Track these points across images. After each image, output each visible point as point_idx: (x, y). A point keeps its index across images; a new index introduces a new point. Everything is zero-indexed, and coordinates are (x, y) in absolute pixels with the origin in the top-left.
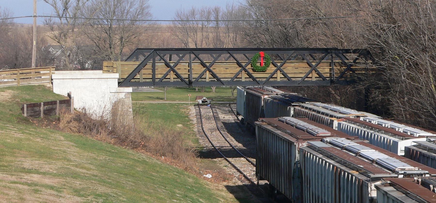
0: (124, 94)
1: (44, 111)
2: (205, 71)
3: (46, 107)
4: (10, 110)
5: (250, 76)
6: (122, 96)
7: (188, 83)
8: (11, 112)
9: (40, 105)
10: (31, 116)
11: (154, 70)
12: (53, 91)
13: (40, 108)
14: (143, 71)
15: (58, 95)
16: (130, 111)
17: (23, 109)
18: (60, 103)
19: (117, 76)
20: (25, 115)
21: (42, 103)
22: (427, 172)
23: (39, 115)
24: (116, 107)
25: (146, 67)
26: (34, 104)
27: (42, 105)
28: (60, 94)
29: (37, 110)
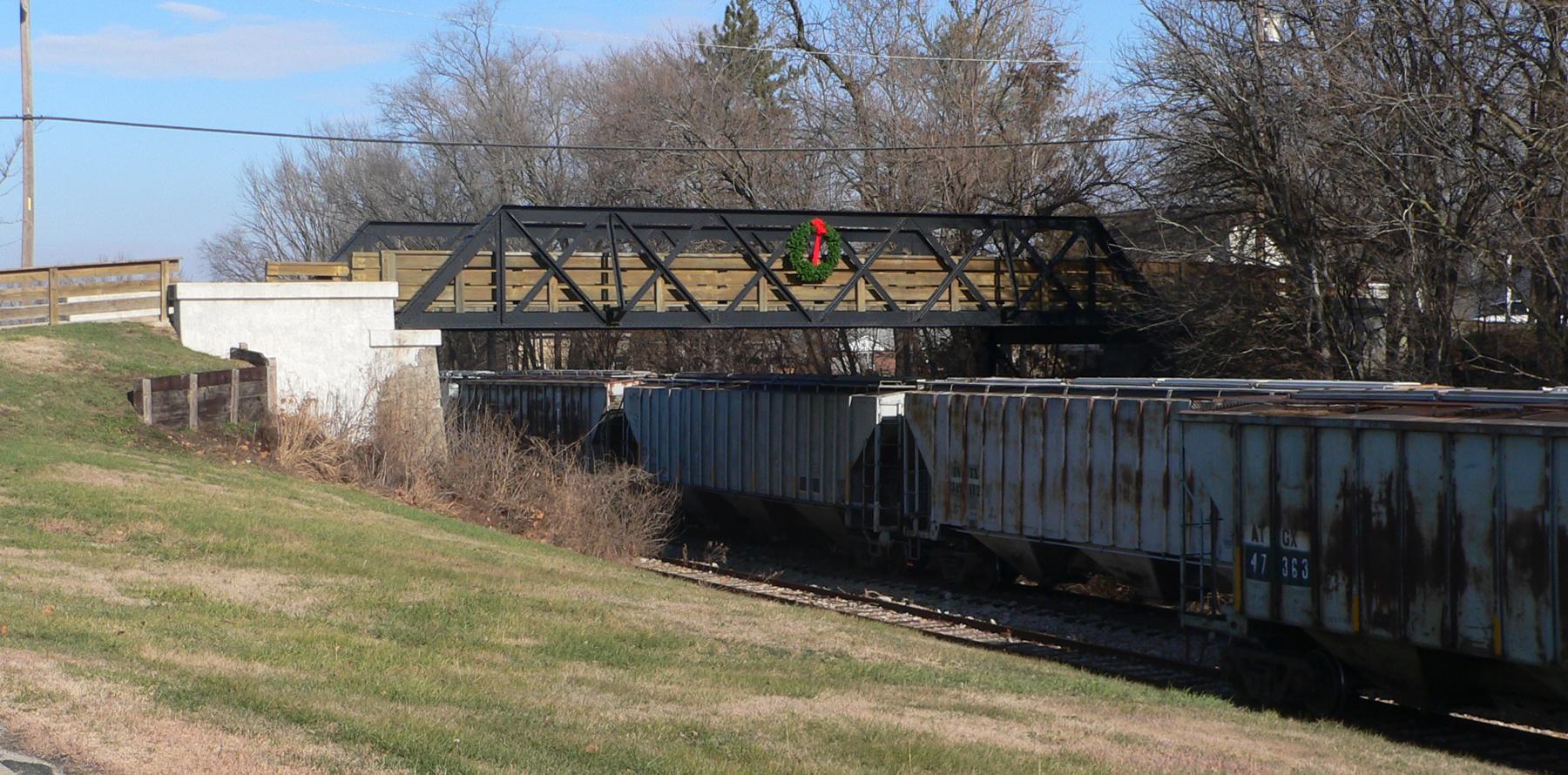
0: (414, 351)
1: (200, 404)
2: (652, 282)
3: (203, 389)
4: (89, 402)
5: (782, 294)
6: (410, 357)
7: (604, 314)
8: (94, 410)
9: (185, 385)
10: (164, 422)
11: (497, 280)
12: (180, 342)
13: (186, 394)
14: (464, 276)
15: (202, 356)
16: (436, 410)
17: (134, 397)
18: (242, 379)
19: (391, 289)
20: (147, 418)
21: (194, 377)
22: (1325, 538)
23: (184, 419)
24: (390, 397)
25: (475, 262)
26: (170, 378)
27: (235, 383)
28: (203, 351)
29: (179, 401)
